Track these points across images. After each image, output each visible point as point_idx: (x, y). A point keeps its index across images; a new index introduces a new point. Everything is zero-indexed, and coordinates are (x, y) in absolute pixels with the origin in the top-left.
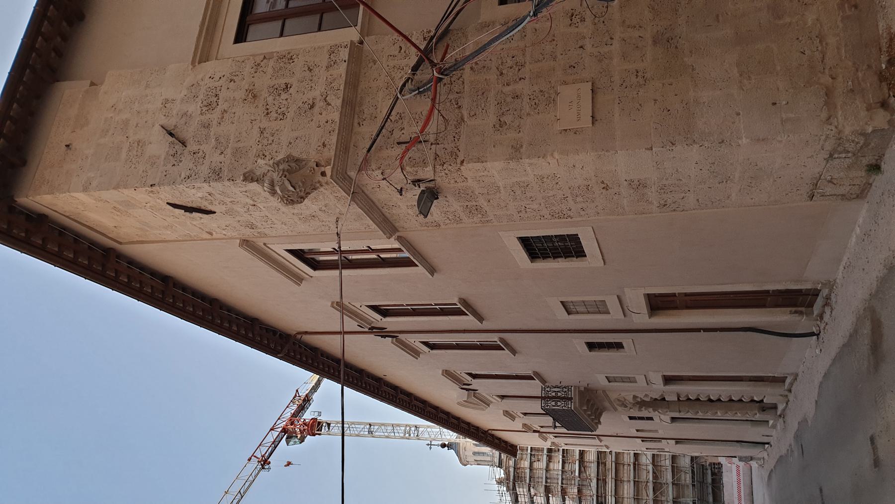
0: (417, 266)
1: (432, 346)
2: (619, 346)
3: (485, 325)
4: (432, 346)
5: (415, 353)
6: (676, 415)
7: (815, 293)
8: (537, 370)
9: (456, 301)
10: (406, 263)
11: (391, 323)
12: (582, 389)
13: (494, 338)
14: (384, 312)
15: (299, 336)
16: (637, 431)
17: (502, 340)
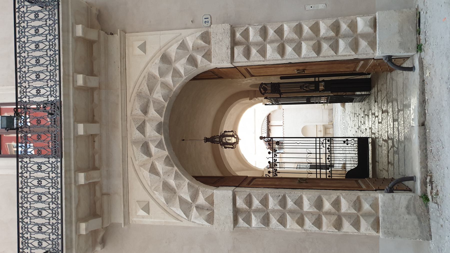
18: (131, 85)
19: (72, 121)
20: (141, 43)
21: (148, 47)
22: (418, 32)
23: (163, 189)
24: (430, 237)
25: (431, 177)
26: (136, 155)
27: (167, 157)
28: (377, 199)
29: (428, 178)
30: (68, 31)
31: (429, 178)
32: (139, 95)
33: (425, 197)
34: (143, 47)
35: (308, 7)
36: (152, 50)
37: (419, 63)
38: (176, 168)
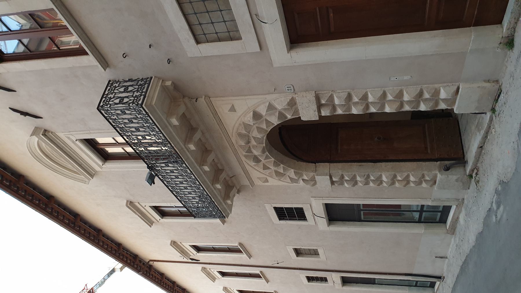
0: (87, 54)
1: (223, 274)
2: (324, 280)
3: (252, 262)
4: (223, 274)
5: (213, 279)
6: (345, 197)
7: (447, 210)
8: (242, 242)
9: (237, 245)
10: (240, 252)
11: (202, 256)
12: (169, 83)
13: (256, 271)
14: (198, 249)
15: (151, 263)
16: (298, 252)
17: (261, 272)
18: (230, 130)
19: (198, 167)
20: (230, 106)
21: (236, 107)
22: (496, 100)
23: (276, 176)
24: (469, 189)
25: (478, 171)
26: (249, 164)
27: (274, 162)
28: (436, 176)
29: (475, 168)
30: (166, 126)
31: (475, 171)
32: (240, 135)
33: (471, 176)
34: (233, 109)
35: (393, 79)
36: (240, 110)
37: (490, 118)
38: (282, 165)
